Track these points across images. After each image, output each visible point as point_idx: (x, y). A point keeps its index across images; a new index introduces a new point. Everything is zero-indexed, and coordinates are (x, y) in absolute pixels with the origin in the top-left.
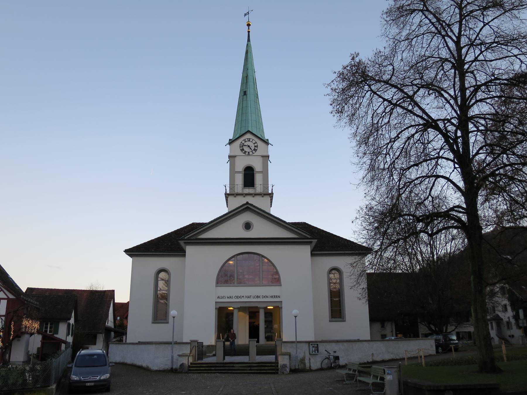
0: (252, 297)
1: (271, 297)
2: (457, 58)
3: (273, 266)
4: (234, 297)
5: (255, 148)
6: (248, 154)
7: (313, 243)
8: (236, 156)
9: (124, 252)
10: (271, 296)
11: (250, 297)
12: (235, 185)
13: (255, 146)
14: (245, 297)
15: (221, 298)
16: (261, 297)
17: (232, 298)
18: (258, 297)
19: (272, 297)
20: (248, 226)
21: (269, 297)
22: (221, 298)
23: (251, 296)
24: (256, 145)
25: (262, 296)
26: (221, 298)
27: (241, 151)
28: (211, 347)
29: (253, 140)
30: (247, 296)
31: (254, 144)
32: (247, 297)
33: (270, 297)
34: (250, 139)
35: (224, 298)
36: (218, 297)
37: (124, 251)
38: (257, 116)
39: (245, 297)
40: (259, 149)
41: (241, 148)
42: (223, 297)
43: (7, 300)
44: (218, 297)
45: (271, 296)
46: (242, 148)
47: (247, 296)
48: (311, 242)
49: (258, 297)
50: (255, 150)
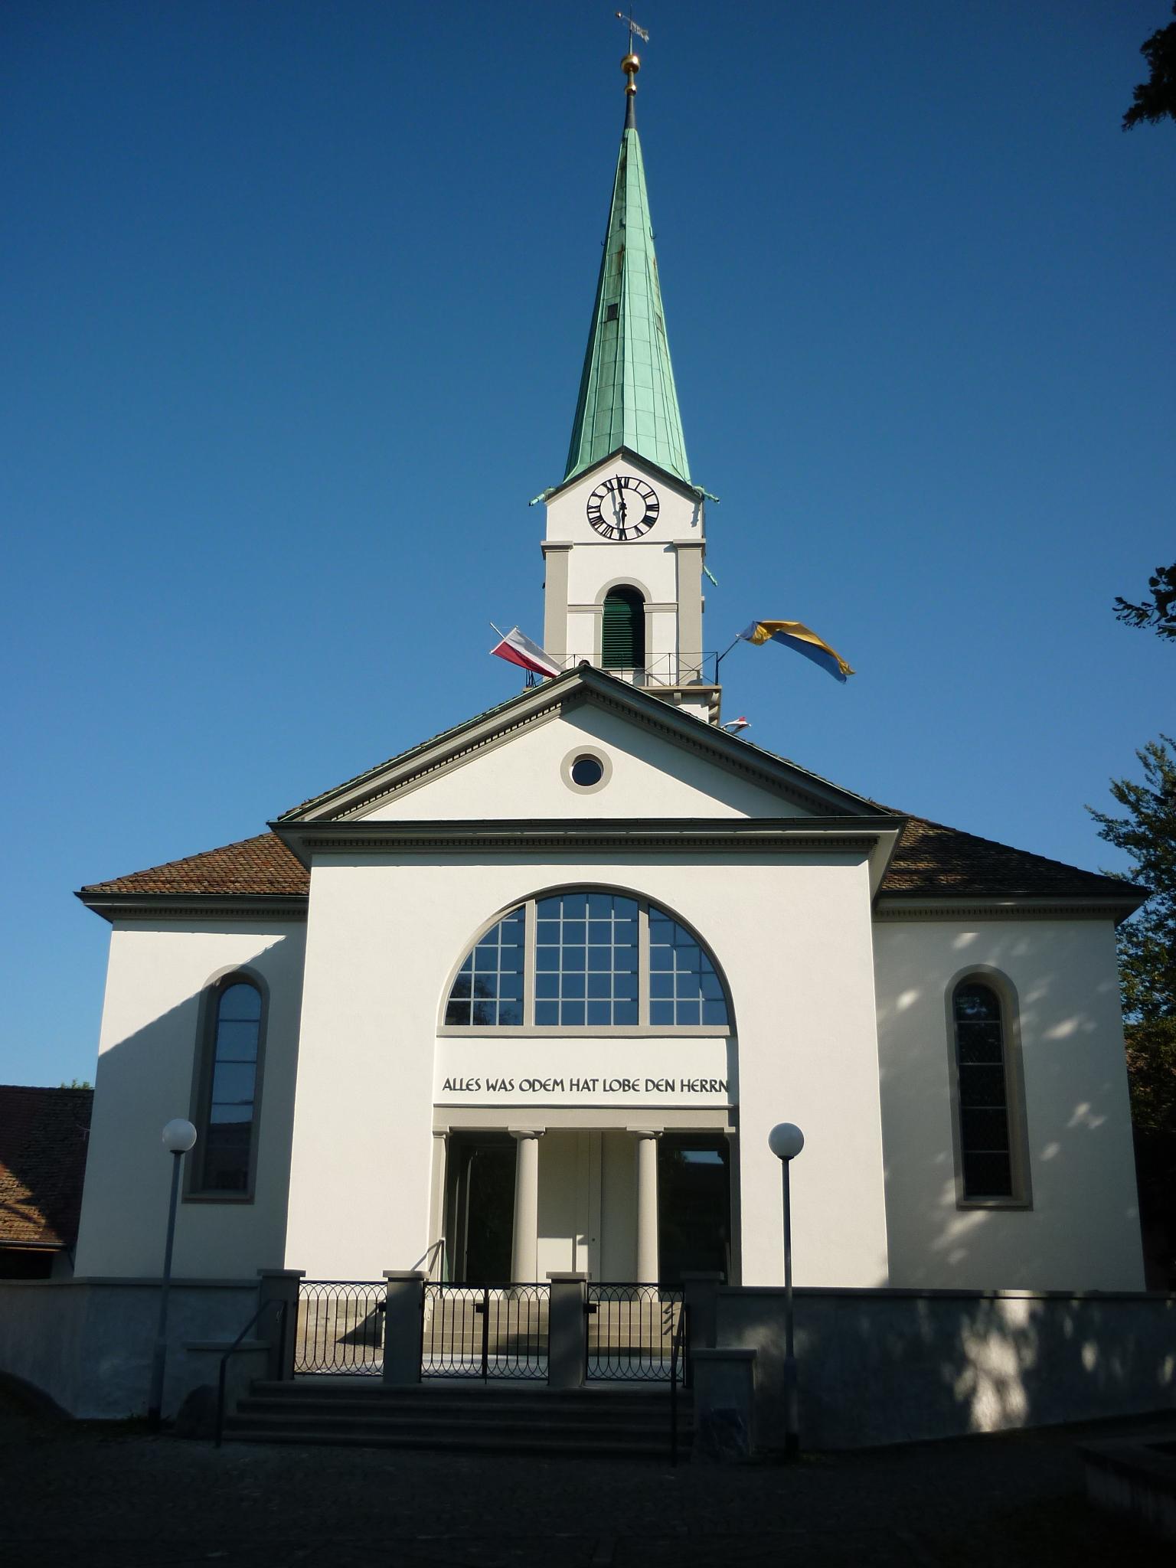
0: (599, 1085)
1: (686, 1088)
2: (1151, 836)
3: (697, 949)
4: (516, 1085)
5: (650, 514)
6: (620, 539)
7: (880, 842)
8: (566, 548)
9: (78, 901)
10: (685, 1083)
11: (591, 1088)
12: (567, 657)
13: (649, 508)
14: (567, 1085)
15: (461, 1089)
16: (642, 1086)
17: (509, 1087)
18: (626, 1085)
19: (691, 1087)
20: (587, 771)
21: (678, 1086)
22: (458, 1087)
23: (594, 1081)
24: (651, 501)
25: (647, 1081)
26: (458, 1087)
27: (593, 525)
28: (922, 1306)
29: (641, 481)
30: (575, 1082)
31: (644, 497)
32: (578, 1085)
33: (682, 1086)
34: (627, 479)
35: (475, 1087)
36: (449, 1086)
37: (77, 894)
38: (658, 397)
39: (567, 1085)
40: (662, 518)
41: (592, 516)
42: (468, 1085)
43: (784, 1285)
44: (449, 1086)
45: (685, 1083)
46: (598, 514)
47: (575, 1082)
48: (873, 841)
49: (626, 1085)
50: (649, 521)
